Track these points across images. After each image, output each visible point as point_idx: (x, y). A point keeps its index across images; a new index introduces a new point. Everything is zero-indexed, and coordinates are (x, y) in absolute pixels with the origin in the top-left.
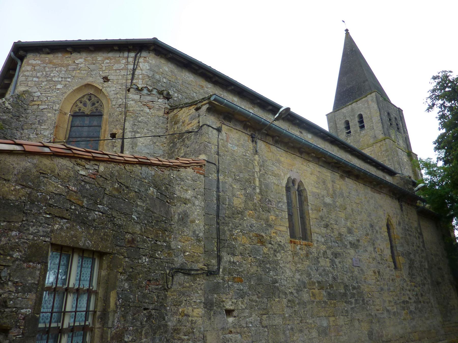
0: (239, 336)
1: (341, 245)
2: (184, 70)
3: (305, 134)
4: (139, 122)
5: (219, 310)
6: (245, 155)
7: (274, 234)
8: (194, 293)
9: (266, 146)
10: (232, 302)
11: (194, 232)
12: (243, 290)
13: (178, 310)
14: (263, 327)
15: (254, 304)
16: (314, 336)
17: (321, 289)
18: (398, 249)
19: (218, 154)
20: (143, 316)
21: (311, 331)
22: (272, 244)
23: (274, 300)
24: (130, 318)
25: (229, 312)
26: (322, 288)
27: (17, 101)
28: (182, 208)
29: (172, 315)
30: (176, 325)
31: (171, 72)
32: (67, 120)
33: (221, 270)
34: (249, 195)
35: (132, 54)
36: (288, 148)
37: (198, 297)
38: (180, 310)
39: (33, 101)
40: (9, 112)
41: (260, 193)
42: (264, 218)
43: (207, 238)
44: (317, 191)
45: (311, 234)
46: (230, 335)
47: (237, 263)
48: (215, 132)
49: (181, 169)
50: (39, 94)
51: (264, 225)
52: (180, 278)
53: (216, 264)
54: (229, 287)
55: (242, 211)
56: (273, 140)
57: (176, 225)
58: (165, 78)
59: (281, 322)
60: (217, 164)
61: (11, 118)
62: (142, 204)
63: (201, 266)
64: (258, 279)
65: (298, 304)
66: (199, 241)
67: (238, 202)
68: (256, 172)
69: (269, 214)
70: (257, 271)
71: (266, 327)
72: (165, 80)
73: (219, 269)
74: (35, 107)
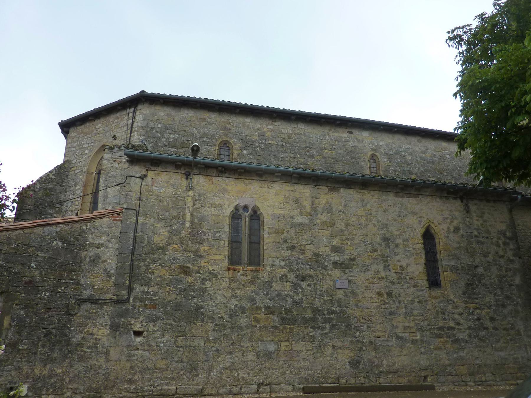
0: (146, 353)
1: (316, 267)
2: (182, 109)
3: (357, 133)
4: (110, 177)
5: (126, 331)
6: (176, 194)
7: (207, 264)
8: (101, 318)
9: (206, 179)
10: (142, 325)
11: (105, 270)
12: (155, 315)
13: (83, 330)
14: (177, 347)
15: (169, 327)
16: (249, 359)
17: (269, 314)
18: (444, 263)
19: (140, 199)
20: (41, 333)
21: (245, 354)
22: (201, 274)
23: (196, 324)
24: (25, 333)
25: (138, 334)
26: (272, 313)
27: (59, 171)
28: (92, 252)
29: (77, 334)
30: (80, 341)
31: (168, 115)
32: (93, 178)
33: (131, 299)
34: (174, 231)
35: (132, 110)
36: (239, 175)
37: (105, 319)
38: (85, 330)
39: (72, 167)
40: (54, 182)
41: (191, 226)
42: (193, 250)
43: (117, 274)
44: (282, 212)
45: (264, 259)
46: (136, 352)
47: (152, 293)
48: (138, 180)
49: (96, 220)
50: (75, 161)
51: (192, 256)
52: (87, 306)
53: (127, 294)
54: (139, 312)
55: (164, 247)
56: (217, 171)
57: (86, 266)
58: (160, 123)
59: (203, 344)
60: (137, 209)
61: (56, 185)
62: (43, 255)
63: (110, 296)
64: (176, 306)
65: (229, 328)
66: (110, 277)
67: (160, 237)
68: (188, 207)
69: (201, 245)
70: (176, 298)
71: (181, 347)
72: (160, 126)
73: (129, 299)
74: (73, 172)
